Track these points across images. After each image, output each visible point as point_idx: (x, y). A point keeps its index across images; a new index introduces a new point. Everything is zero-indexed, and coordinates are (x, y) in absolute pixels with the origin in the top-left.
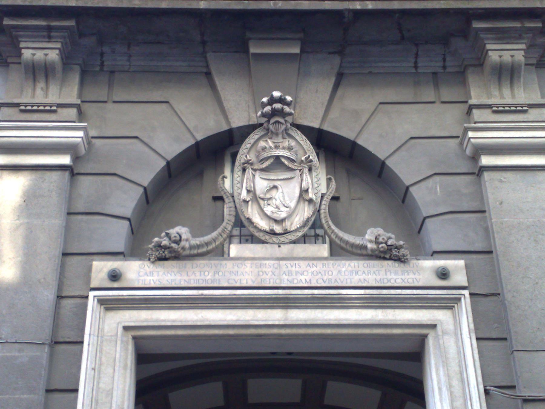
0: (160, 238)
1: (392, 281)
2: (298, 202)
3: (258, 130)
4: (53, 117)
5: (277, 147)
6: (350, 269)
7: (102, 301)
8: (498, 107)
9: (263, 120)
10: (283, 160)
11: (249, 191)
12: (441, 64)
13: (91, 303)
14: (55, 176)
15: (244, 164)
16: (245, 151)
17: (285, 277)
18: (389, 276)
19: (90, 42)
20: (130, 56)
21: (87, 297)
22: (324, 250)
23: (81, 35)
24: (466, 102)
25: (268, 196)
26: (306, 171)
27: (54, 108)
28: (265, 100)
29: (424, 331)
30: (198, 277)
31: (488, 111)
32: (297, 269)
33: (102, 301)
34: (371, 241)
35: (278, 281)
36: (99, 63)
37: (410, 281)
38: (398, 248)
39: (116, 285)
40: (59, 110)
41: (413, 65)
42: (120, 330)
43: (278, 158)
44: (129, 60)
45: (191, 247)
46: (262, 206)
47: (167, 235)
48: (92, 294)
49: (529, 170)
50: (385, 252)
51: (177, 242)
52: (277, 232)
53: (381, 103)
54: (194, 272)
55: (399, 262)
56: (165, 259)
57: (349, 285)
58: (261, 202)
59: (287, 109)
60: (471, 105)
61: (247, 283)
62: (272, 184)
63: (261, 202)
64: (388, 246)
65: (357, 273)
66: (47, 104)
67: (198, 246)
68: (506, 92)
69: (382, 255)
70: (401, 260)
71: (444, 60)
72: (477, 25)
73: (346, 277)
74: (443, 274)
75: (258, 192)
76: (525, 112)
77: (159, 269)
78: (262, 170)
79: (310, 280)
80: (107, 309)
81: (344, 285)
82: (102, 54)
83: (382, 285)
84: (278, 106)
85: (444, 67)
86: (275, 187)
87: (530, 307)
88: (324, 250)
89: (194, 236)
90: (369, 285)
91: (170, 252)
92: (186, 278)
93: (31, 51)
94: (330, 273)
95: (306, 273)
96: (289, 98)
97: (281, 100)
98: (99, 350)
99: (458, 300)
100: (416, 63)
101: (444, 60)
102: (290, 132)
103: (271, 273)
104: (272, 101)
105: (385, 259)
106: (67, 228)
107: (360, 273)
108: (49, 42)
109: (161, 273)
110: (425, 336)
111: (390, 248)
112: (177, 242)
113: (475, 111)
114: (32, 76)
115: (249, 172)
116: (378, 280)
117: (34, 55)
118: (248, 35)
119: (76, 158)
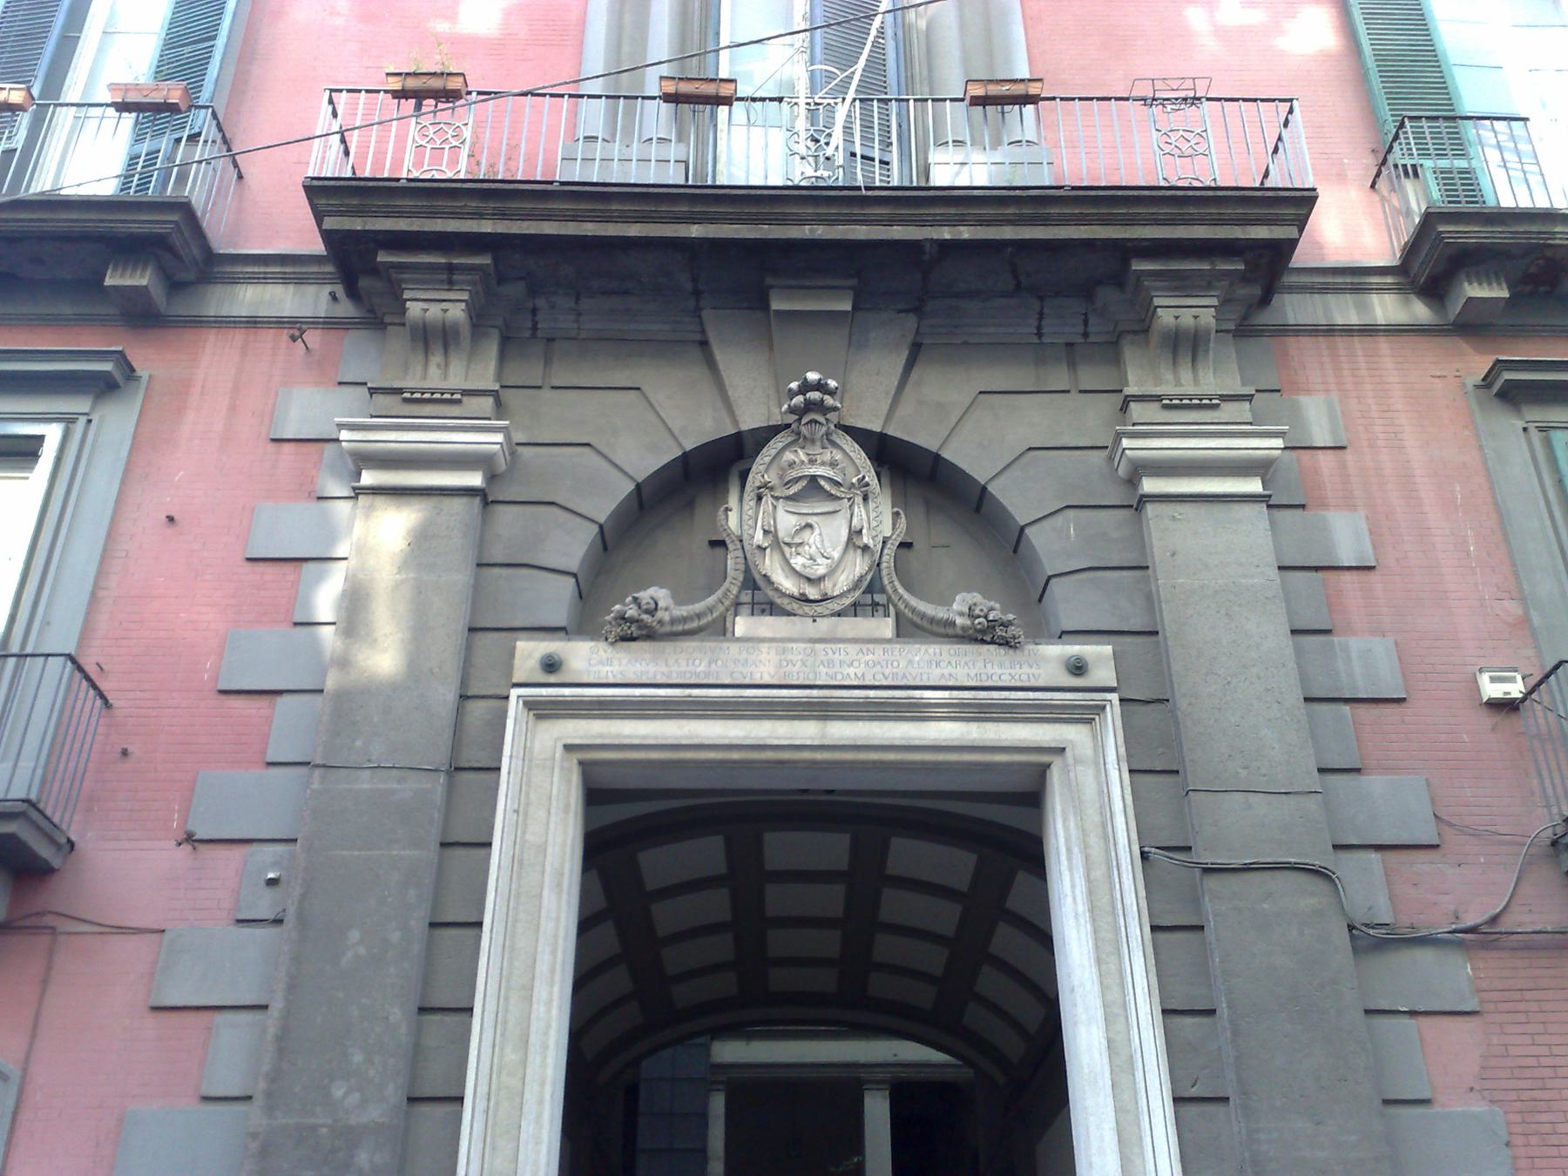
5: (812, 462)
7: (530, 705)
9: (791, 418)
10: (822, 483)
11: (766, 532)
12: (1080, 329)
13: (513, 706)
14: (458, 504)
19: (515, 290)
20: (579, 314)
21: (507, 698)
25: (797, 540)
26: (859, 499)
27: (457, 396)
29: (1045, 758)
31: (1156, 405)
32: (842, 657)
34: (961, 614)
35: (811, 676)
36: (529, 324)
38: (1006, 625)
39: (552, 679)
44: (577, 321)
45: (673, 621)
46: (788, 556)
48: (514, 692)
50: (983, 631)
53: (981, 393)
56: (632, 639)
58: (786, 549)
59: (829, 401)
60: (1127, 396)
63: (786, 549)
64: (988, 621)
65: (938, 664)
67: (685, 620)
71: (1086, 323)
72: (1138, 266)
73: (921, 671)
77: (621, 655)
78: (788, 498)
79: (863, 675)
80: (539, 717)
82: (534, 311)
84: (814, 395)
85: (1085, 335)
86: (809, 526)
89: (679, 601)
91: (640, 628)
92: (665, 669)
94: (895, 664)
95: (856, 664)
96: (832, 383)
97: (820, 386)
98: (525, 783)
100: (1039, 328)
101: (1086, 323)
102: (834, 437)
103: (799, 663)
104: (806, 387)
105: (983, 642)
110: (1048, 766)
111: (992, 625)
118: (769, 281)
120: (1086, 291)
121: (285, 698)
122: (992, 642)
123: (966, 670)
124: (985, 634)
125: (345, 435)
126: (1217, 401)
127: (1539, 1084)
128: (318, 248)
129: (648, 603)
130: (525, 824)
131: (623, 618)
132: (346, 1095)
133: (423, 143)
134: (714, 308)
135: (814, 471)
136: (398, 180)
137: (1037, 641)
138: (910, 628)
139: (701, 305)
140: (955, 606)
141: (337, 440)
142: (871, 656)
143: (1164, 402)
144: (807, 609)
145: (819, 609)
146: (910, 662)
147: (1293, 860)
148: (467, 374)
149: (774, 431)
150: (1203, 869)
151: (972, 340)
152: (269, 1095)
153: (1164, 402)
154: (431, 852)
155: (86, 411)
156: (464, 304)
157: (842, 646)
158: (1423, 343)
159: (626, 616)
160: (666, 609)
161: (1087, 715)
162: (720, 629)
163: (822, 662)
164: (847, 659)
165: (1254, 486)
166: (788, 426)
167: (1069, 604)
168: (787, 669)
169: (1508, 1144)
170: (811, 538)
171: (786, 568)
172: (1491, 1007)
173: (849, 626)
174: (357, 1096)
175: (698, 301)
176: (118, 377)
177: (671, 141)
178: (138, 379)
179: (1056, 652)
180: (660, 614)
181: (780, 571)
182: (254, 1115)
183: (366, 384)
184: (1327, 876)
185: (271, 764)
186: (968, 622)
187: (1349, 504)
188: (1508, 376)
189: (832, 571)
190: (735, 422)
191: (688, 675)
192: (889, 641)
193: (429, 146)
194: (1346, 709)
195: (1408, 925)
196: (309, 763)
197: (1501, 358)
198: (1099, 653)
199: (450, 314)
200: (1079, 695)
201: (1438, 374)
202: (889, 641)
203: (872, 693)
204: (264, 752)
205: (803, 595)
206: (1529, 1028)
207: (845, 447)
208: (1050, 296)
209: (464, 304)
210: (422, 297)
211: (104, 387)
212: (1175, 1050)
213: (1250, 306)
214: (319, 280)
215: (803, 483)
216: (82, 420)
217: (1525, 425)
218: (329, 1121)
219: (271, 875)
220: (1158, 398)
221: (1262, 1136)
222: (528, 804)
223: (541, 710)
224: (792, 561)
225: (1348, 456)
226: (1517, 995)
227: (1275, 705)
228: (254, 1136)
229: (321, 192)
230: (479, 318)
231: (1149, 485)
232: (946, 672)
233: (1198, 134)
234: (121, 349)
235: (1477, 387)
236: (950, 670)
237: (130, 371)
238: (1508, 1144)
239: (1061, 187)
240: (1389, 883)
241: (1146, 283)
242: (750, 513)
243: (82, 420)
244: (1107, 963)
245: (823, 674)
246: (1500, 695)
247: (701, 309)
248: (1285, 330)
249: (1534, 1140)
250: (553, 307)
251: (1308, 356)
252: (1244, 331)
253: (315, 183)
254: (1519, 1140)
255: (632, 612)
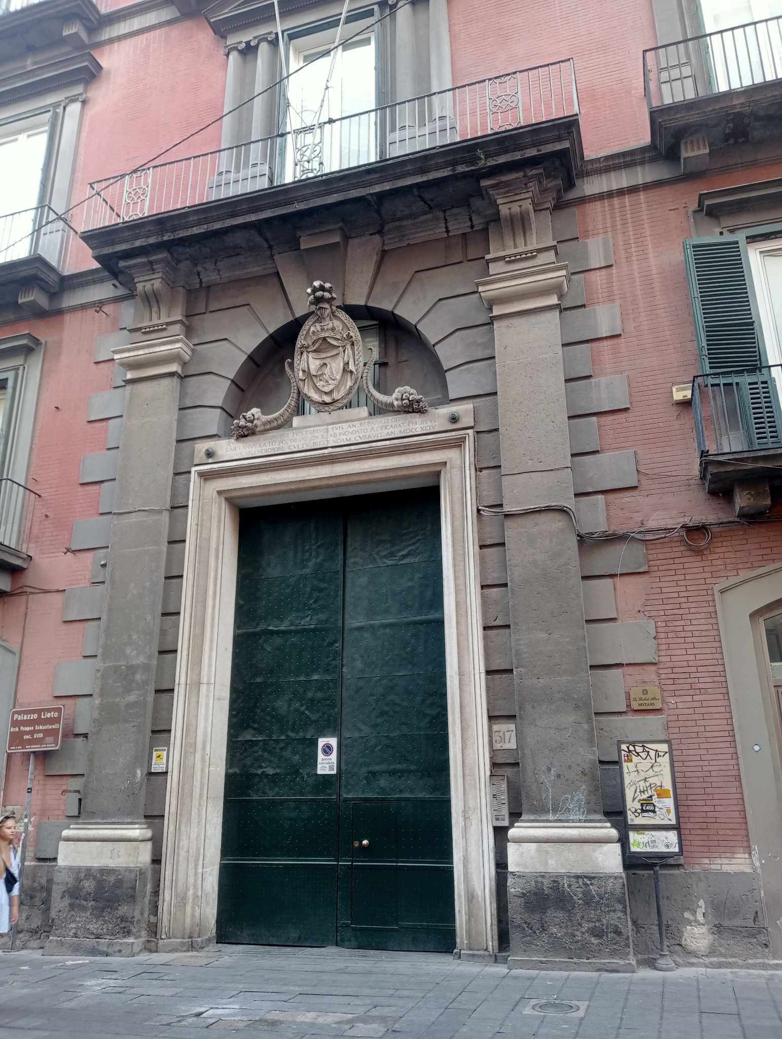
0: (239, 419)
1: (413, 430)
2: (342, 375)
3: (311, 317)
4: (164, 334)
5: (322, 330)
6: (381, 425)
7: (201, 475)
8: (510, 258)
9: (313, 308)
10: (329, 340)
11: (304, 371)
12: (469, 224)
13: (194, 476)
14: (166, 382)
15: (300, 348)
16: (303, 337)
17: (331, 439)
18: (411, 427)
19: (185, 266)
20: (219, 271)
21: (189, 472)
22: (364, 411)
23: (179, 262)
24: (484, 257)
25: (320, 373)
26: (349, 347)
27: (164, 326)
28: (309, 291)
29: (437, 469)
30: (268, 447)
31: (501, 263)
32: (341, 431)
33: (201, 475)
34: (397, 399)
35: (326, 443)
36: (198, 281)
37: (428, 428)
38: (418, 401)
39: (210, 461)
40: (169, 328)
41: (445, 230)
42: (215, 494)
43: (324, 339)
44: (219, 274)
45: (264, 424)
46: (315, 382)
47: (244, 417)
48: (194, 469)
49: (508, 317)
50: (408, 406)
51: (252, 422)
52: (327, 401)
53: (416, 272)
54: (264, 444)
55: (420, 413)
56: (246, 436)
57: (380, 438)
58: (314, 379)
59: (327, 295)
60: (487, 260)
61: (303, 447)
62: (322, 362)
63: (314, 379)
64: (410, 401)
65: (386, 428)
66: (774, 222)
67: (270, 422)
68: (520, 240)
69: (407, 409)
70: (421, 411)
71: (471, 219)
72: (484, 183)
73: (378, 432)
74: (454, 419)
75: (313, 372)
76: (533, 257)
77: (240, 445)
78: (315, 351)
79: (350, 439)
80: (206, 480)
81: (375, 439)
82: (198, 274)
83: (405, 435)
84: (319, 294)
85: (472, 227)
86: (325, 364)
87: (519, 436)
88: (364, 411)
89: (263, 413)
90: (396, 436)
91: (248, 430)
92: (260, 449)
93: (143, 284)
94: (365, 430)
95: (347, 433)
96: (327, 285)
97: (322, 288)
98: (200, 509)
99: (463, 439)
100: (447, 228)
101: (471, 219)
102: (337, 314)
103: (321, 437)
104: (315, 290)
105: (409, 412)
106: (180, 421)
107: (388, 427)
108: (154, 273)
109: (241, 447)
110: (440, 472)
111: (411, 402)
112: (252, 422)
113: (490, 265)
114: (512, 235)
115: (305, 354)
116: (402, 430)
117: (145, 286)
118: (299, 233)
119: (184, 364)
120: (465, 201)
121: (106, 484)
122: (413, 412)
123: (399, 429)
124: (411, 408)
125: (116, 357)
126: (536, 253)
127: (678, 606)
128: (96, 265)
129: (249, 417)
130: (201, 530)
131: (240, 427)
132: (131, 652)
133: (129, 201)
134: (279, 253)
135: (323, 335)
136: (118, 224)
137: (437, 407)
138: (379, 410)
139: (273, 253)
140: (393, 396)
141: (113, 360)
142: (354, 428)
143: (506, 259)
144: (326, 408)
145: (332, 408)
146: (372, 429)
147: (532, 507)
148: (169, 314)
149: (306, 317)
150: (505, 515)
151: (412, 242)
152: (103, 654)
153: (506, 259)
154: (164, 547)
155: (22, 363)
156: (160, 279)
157: (340, 425)
158: (666, 191)
159: (240, 425)
160: (258, 419)
161: (458, 444)
162: (285, 424)
163: (331, 435)
164: (343, 431)
165: (553, 300)
166: (314, 312)
167: (457, 384)
168: (315, 441)
169: (655, 638)
170: (327, 371)
171: (315, 388)
172: (656, 568)
173: (346, 413)
174: (135, 652)
175: (271, 252)
176: (31, 344)
177: (231, 172)
178: (41, 344)
179: (446, 411)
180: (255, 422)
181: (312, 390)
182: (98, 663)
183: (126, 328)
184: (565, 511)
185: (102, 514)
186: (400, 404)
187: (610, 298)
188: (707, 203)
189: (337, 387)
190: (293, 313)
191: (276, 450)
192: (364, 419)
193: (132, 203)
194: (594, 419)
195: (196, 527)
196: (111, 513)
197: (702, 192)
198: (464, 409)
199: (155, 286)
200: (453, 433)
201: (673, 208)
202: (364, 419)
203: (352, 448)
204: (98, 510)
205: (323, 401)
206: (676, 578)
207: (342, 318)
208: (449, 209)
209: (160, 279)
210: (142, 280)
211: (28, 351)
212: (485, 603)
213: (559, 191)
214: (102, 281)
215: (320, 342)
216: (21, 368)
217: (722, 230)
218: (125, 663)
219: (102, 563)
220: (503, 258)
221: (522, 642)
222: (202, 521)
223: (206, 476)
224: (317, 384)
225: (614, 270)
226: (672, 561)
227: (551, 423)
228: (98, 671)
229: (90, 238)
230: (171, 284)
231: (497, 311)
232: (390, 431)
233: (513, 95)
234: (27, 332)
235: (695, 212)
236: (392, 430)
237: (37, 342)
238: (655, 638)
239: (434, 148)
240: (607, 510)
241: (490, 192)
242: (298, 362)
243: (21, 368)
244: (459, 566)
245: (331, 441)
246: (681, 398)
247: (274, 255)
248: (584, 200)
249: (670, 635)
250: (206, 269)
251: (597, 212)
252: (560, 206)
253: (84, 235)
254: (662, 635)
255: (242, 422)
